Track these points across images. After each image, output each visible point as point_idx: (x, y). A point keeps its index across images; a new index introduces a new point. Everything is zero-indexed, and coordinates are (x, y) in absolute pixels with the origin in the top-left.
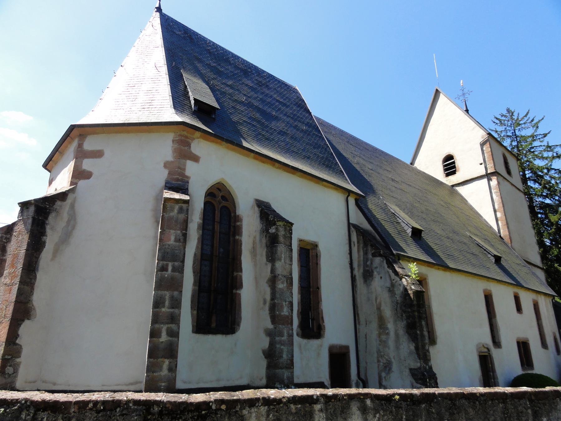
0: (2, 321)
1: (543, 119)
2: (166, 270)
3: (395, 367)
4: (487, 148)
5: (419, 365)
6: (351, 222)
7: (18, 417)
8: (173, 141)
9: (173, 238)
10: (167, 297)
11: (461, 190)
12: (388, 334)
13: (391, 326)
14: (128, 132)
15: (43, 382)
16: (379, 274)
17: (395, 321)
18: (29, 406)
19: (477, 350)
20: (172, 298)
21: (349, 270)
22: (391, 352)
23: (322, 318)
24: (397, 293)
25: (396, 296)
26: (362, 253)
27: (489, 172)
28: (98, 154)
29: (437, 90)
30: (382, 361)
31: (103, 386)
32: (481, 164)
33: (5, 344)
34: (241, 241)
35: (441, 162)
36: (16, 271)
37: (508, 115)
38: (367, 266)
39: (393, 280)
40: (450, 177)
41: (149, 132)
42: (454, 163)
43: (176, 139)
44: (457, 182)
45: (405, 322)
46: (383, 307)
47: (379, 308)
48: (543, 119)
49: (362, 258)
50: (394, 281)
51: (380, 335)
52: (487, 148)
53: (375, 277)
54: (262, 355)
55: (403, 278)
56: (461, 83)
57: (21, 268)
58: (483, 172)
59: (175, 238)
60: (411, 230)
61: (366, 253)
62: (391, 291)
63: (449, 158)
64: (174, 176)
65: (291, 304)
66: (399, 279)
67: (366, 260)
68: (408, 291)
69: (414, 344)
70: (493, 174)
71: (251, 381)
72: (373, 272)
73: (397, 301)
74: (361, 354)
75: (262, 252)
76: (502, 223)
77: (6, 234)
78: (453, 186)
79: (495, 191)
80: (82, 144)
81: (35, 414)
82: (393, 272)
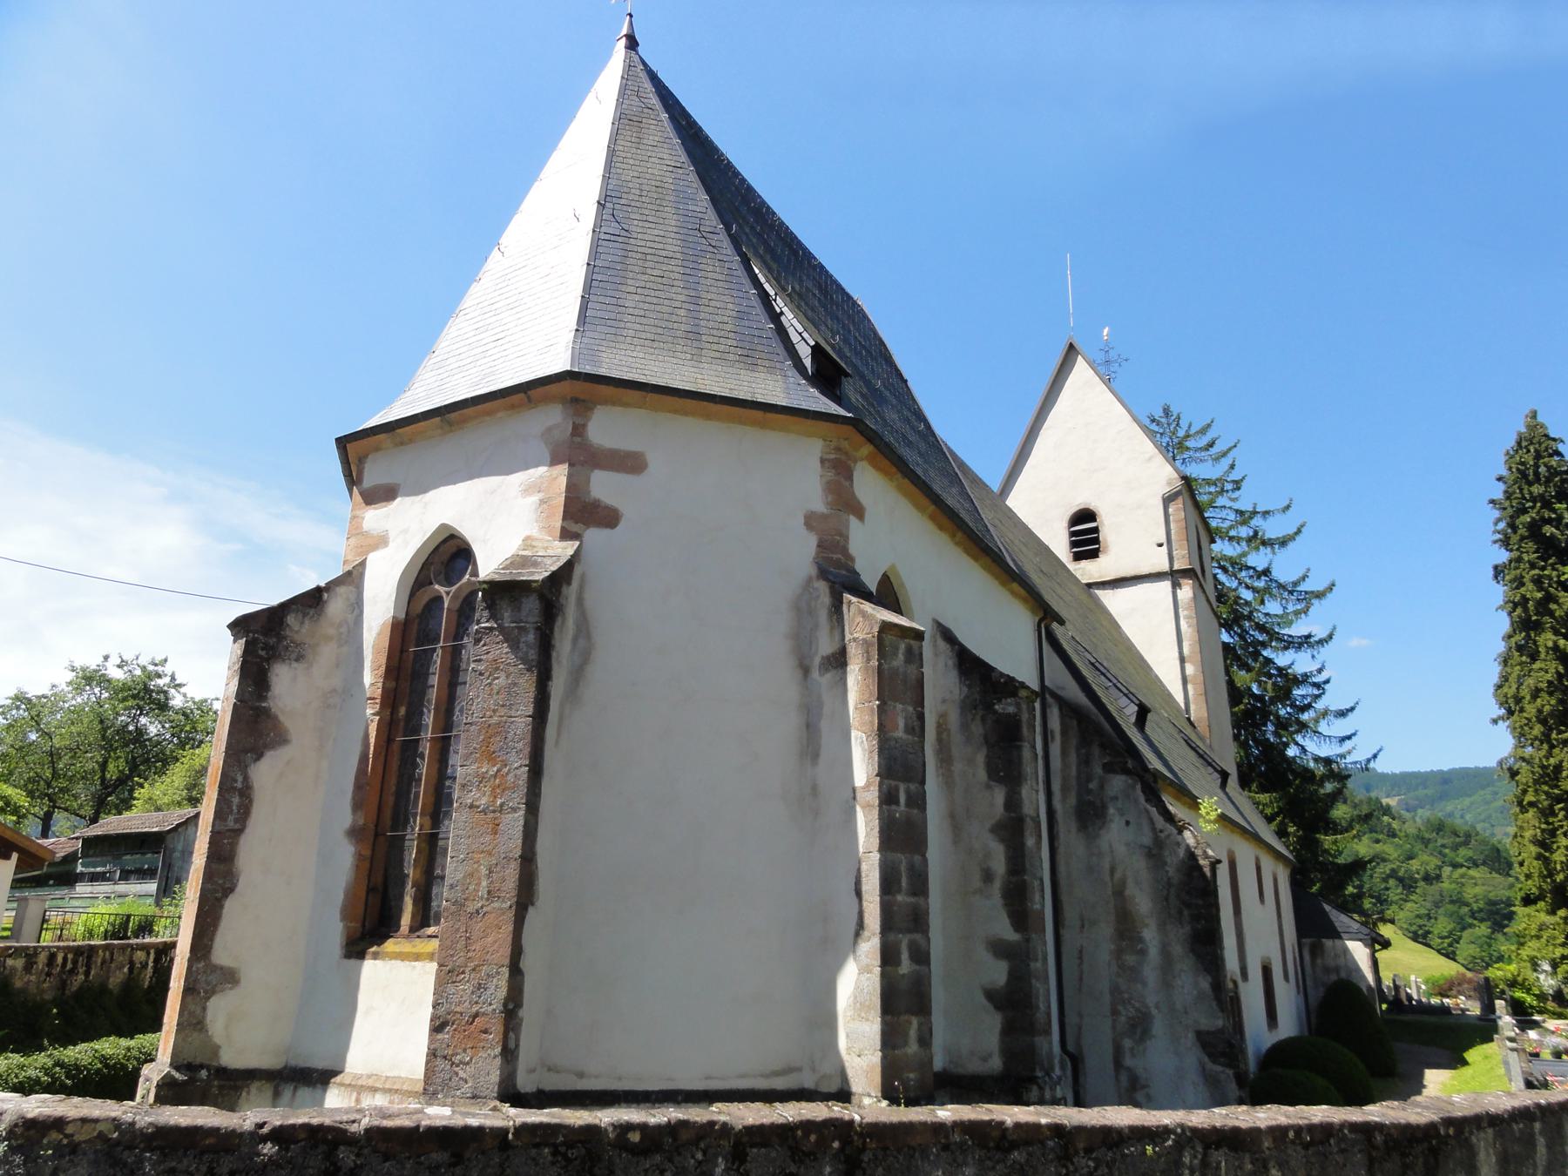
0: (482, 907)
1: (1235, 446)
2: (897, 803)
3: (1158, 1027)
4: (1176, 508)
5: (1220, 1023)
6: (1047, 683)
7: (1178, 1163)
8: (822, 461)
10: (903, 868)
11: (1109, 598)
12: (1143, 953)
13: (1150, 935)
14: (708, 416)
15: (549, 1070)
16: (1122, 815)
17: (1162, 927)
18: (1190, 1139)
20: (911, 868)
22: (1150, 993)
24: (1169, 860)
25: (1167, 868)
26: (1073, 758)
27: (1176, 567)
28: (630, 463)
29: (1071, 346)
30: (1124, 1013)
31: (707, 1078)
32: (1160, 545)
33: (510, 971)
35: (1065, 524)
36: (507, 774)
37: (1163, 420)
38: (1089, 792)
39: (1161, 831)
40: (1084, 564)
41: (762, 425)
42: (1096, 530)
43: (828, 457)
44: (1100, 577)
45: (1187, 928)
46: (1131, 890)
47: (1119, 892)
48: (1235, 446)
49: (1074, 772)
50: (1162, 835)
51: (1118, 954)
52: (1178, 509)
53: (1111, 821)
54: (982, 1000)
55: (1187, 828)
56: (1105, 333)
57: (526, 766)
58: (1164, 566)
59: (906, 725)
60: (1136, 708)
61: (1085, 761)
62: (1154, 855)
63: (1085, 516)
64: (832, 553)
65: (1041, 880)
66: (1175, 831)
67: (1084, 778)
68: (1197, 860)
69: (1209, 979)
70: (1186, 573)
71: (951, 1062)
72: (1104, 807)
73: (1169, 879)
74: (1067, 993)
76: (1195, 689)
77: (265, 635)
78: (1089, 585)
79: (1186, 613)
80: (584, 426)
81: (1205, 1155)
82: (1159, 813)
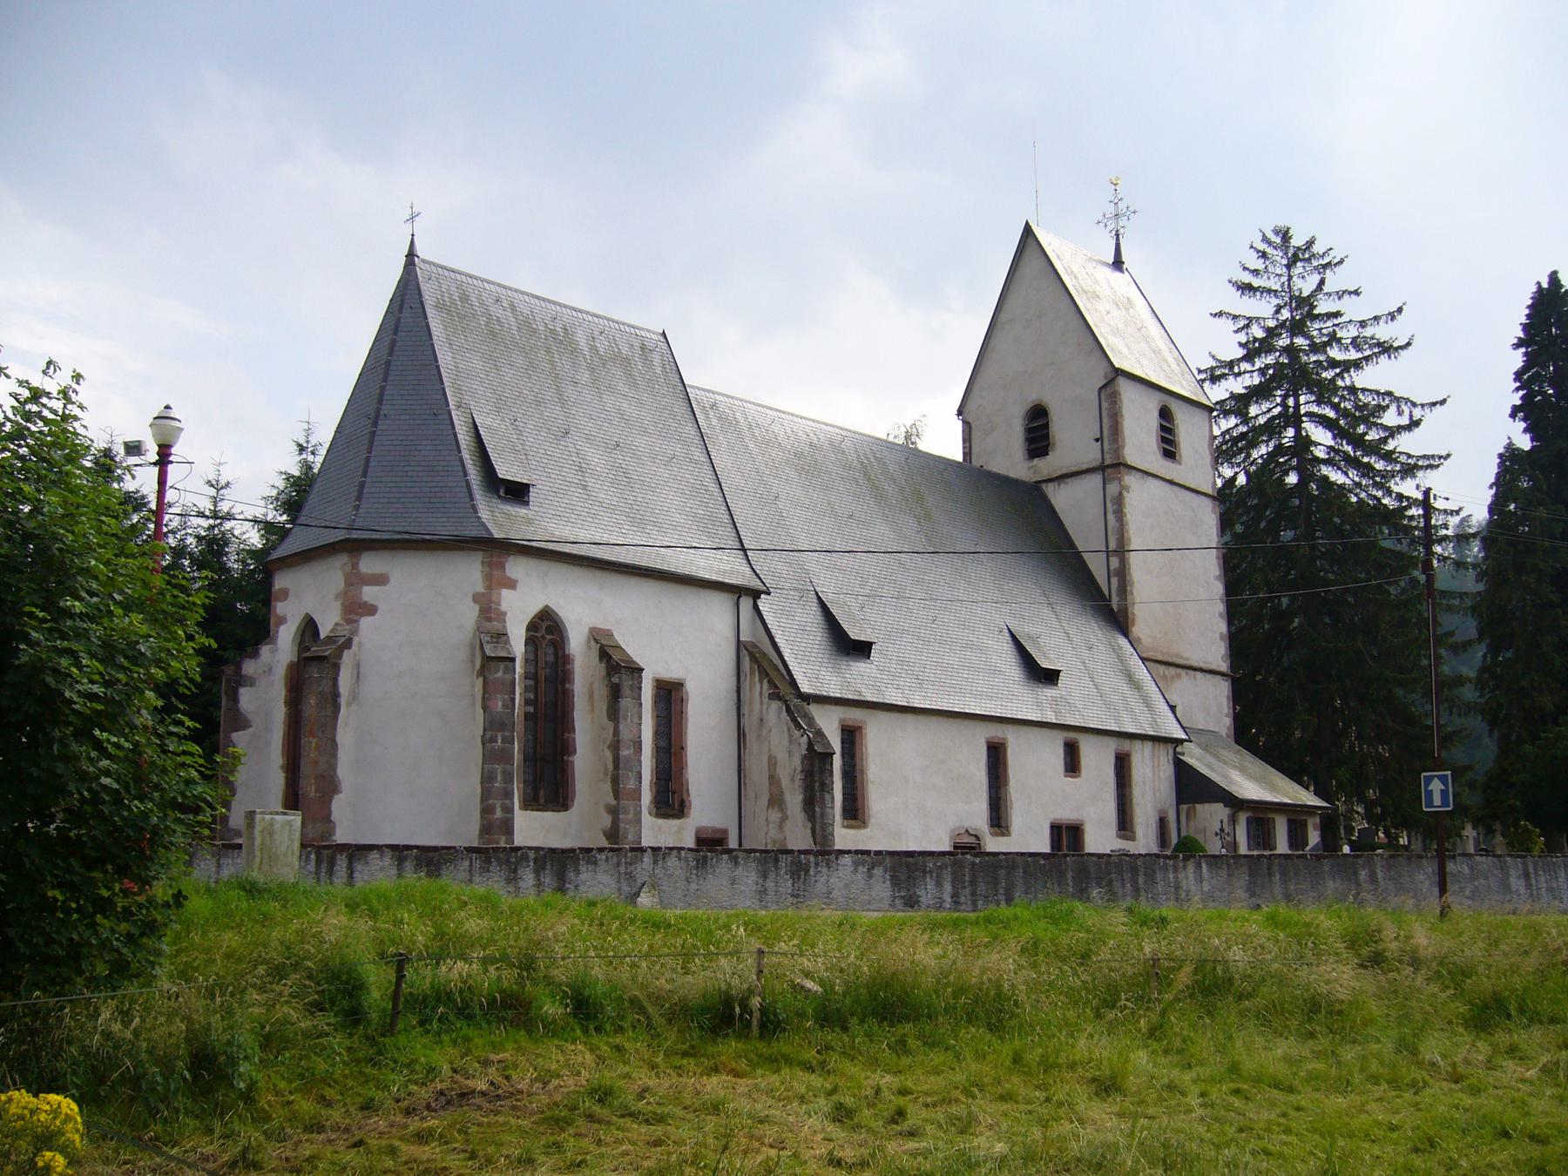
6: (741, 639)
9: (500, 704)
19: (951, 838)
20: (504, 772)
21: (735, 717)
23: (688, 790)
28: (381, 580)
34: (573, 691)
75: (602, 707)
